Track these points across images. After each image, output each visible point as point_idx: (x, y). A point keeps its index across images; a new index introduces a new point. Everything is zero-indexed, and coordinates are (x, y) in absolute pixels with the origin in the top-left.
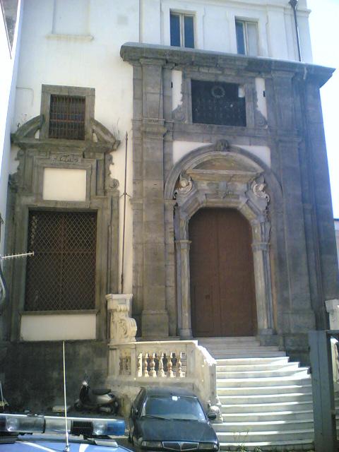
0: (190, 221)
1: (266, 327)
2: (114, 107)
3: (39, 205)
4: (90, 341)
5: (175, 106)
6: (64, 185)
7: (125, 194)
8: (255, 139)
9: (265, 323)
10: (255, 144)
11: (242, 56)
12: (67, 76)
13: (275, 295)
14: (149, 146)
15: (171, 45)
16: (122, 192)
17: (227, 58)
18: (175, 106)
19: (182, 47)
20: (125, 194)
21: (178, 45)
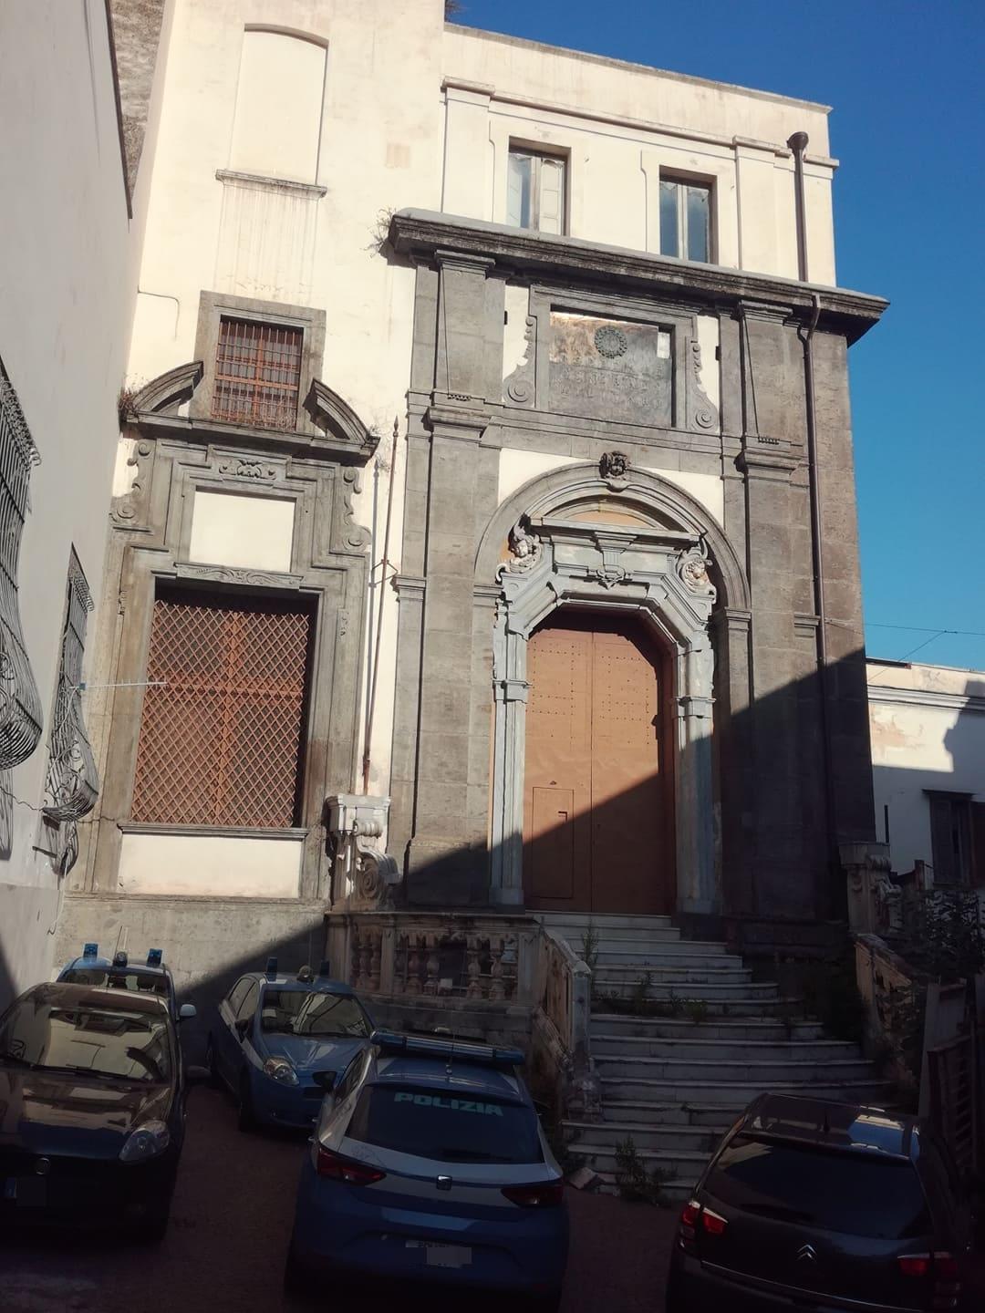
0: (472, 27)
1: (696, 894)
2: (370, 354)
3: (183, 573)
4: (283, 902)
5: (508, 369)
6: (240, 534)
7: (385, 562)
8: (689, 455)
9: (696, 885)
10: (693, 469)
11: (803, 284)
12: (267, 284)
13: (816, 1094)
14: (446, 456)
15: (837, 286)
16: (379, 557)
17: (489, 223)
18: (508, 369)
19: (682, 257)
20: (385, 562)
21: (674, 253)
